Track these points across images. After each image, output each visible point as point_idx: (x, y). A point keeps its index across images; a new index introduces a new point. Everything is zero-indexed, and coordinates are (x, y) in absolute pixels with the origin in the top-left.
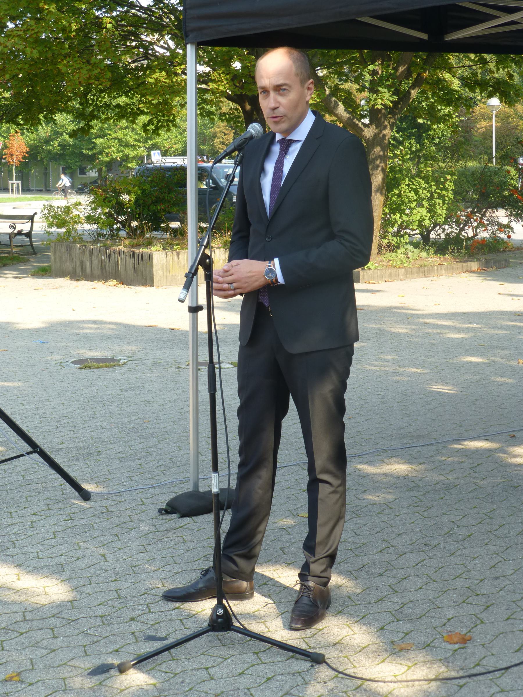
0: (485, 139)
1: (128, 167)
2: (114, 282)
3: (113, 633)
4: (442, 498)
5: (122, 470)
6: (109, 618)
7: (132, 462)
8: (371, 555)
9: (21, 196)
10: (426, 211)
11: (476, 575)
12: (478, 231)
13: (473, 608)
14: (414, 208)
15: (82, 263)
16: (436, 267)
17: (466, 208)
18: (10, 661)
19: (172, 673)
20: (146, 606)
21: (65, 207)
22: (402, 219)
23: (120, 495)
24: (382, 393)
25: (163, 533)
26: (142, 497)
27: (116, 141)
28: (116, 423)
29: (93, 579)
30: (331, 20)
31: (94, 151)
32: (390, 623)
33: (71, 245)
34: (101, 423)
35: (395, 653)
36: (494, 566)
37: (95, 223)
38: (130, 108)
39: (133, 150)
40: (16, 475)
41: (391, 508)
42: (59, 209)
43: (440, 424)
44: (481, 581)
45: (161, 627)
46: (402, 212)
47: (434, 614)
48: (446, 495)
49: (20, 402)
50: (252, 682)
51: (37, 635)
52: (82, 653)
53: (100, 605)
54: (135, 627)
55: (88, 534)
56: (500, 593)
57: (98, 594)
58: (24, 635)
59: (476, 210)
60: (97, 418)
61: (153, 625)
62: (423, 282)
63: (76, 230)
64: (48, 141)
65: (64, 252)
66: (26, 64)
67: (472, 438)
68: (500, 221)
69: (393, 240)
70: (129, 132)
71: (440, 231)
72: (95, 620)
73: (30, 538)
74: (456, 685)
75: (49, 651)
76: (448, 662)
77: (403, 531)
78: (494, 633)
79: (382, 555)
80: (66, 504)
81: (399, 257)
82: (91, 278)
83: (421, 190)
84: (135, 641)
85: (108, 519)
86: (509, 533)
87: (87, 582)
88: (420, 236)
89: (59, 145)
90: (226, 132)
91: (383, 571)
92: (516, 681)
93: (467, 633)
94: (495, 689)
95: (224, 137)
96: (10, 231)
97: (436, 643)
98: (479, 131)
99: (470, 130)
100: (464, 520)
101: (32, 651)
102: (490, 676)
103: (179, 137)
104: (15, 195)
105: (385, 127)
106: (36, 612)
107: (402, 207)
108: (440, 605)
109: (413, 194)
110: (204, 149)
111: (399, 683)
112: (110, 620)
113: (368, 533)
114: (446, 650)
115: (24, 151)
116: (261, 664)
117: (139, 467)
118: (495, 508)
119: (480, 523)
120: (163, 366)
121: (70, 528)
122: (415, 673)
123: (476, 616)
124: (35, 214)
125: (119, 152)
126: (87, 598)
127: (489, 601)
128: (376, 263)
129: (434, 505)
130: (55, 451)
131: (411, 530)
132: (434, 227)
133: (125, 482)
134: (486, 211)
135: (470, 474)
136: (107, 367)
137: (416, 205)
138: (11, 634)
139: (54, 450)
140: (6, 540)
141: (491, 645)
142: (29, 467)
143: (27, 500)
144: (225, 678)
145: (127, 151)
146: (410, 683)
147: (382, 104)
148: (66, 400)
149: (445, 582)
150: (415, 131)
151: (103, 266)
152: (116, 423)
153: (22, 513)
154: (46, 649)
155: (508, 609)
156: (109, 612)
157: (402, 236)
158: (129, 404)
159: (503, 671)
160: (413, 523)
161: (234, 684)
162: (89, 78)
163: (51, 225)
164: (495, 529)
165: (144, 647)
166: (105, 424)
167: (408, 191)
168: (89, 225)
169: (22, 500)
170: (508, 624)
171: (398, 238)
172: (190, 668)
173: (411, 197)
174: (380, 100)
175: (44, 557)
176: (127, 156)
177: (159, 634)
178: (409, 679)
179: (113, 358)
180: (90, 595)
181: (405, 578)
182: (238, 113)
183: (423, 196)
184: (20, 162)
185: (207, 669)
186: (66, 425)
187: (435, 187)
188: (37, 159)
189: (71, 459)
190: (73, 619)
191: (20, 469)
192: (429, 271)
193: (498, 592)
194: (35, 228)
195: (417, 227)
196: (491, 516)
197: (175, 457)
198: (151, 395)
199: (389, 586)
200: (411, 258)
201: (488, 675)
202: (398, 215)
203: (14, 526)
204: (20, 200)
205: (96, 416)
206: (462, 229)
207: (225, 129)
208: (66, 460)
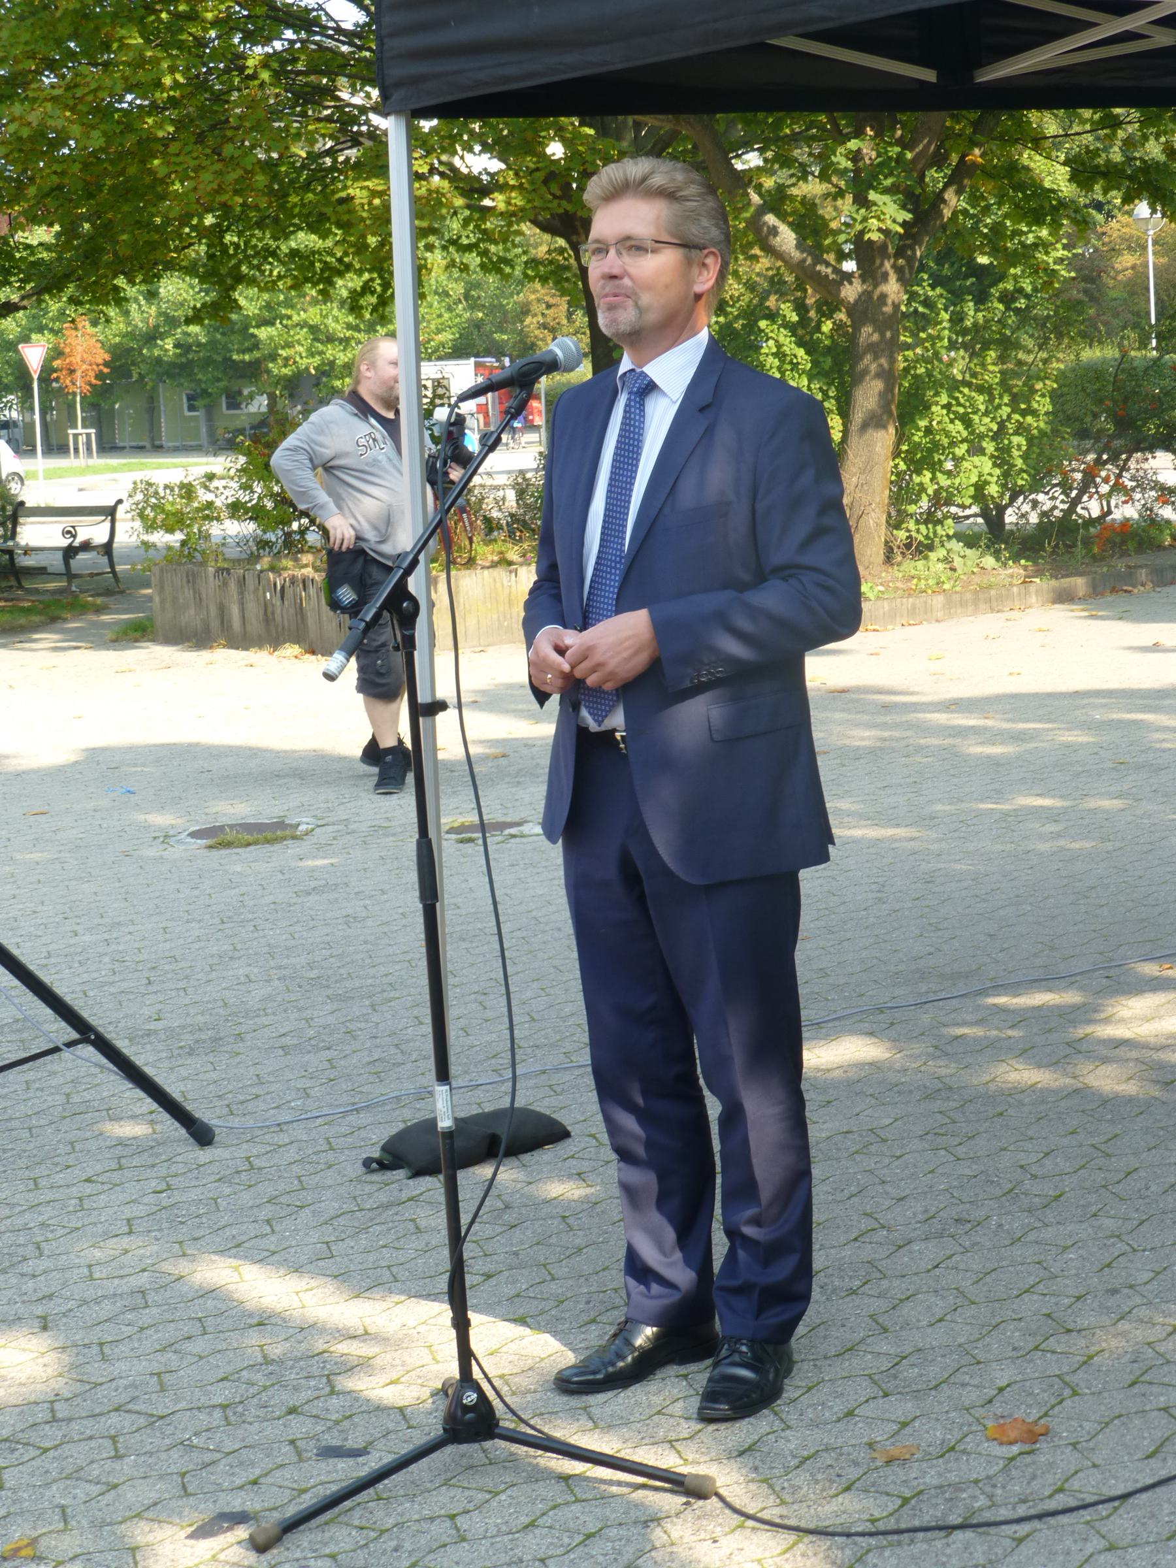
0: (1132, 294)
1: (332, 387)
2: (295, 649)
3: (249, 1441)
4: (1001, 1114)
5: (288, 1075)
6: (240, 1409)
7: (312, 1055)
8: (834, 1247)
9: (97, 461)
10: (990, 464)
11: (1066, 1286)
12: (1113, 503)
13: (1057, 1361)
14: (963, 458)
15: (222, 611)
16: (1015, 589)
17: (1086, 452)
18: (16, 1514)
19: (373, 1530)
20: (324, 1380)
21: (182, 486)
22: (938, 483)
23: (281, 1130)
24: (880, 879)
25: (371, 1214)
26: (329, 1135)
27: (305, 330)
28: (280, 967)
29: (210, 1322)
30: (697, 50)
31: (257, 354)
32: (867, 1401)
33: (196, 569)
34: (247, 970)
35: (877, 1468)
36: (1109, 1266)
37: (251, 519)
38: (320, 261)
39: (345, 350)
40: (52, 1094)
41: (884, 1141)
42: (168, 491)
43: (1005, 946)
44: (1078, 1298)
45: (355, 1425)
46: (935, 467)
47: (967, 1377)
48: (1010, 1106)
49: (68, 928)
50: (551, 1544)
51: (77, 1454)
52: (177, 1491)
53: (222, 1380)
54: (299, 1427)
55: (204, 1220)
56: (1120, 1325)
57: (219, 1356)
58: (51, 1454)
59: (1105, 457)
60: (239, 958)
61: (337, 1422)
62: (987, 623)
63: (207, 537)
64: (152, 337)
65: (182, 587)
66: (74, 161)
67: (1018, 984)
68: (1161, 478)
69: (918, 531)
70: (332, 309)
71: (1026, 508)
72: (210, 1414)
73: (74, 1234)
74: (1009, 1537)
75: (104, 1488)
76: (994, 1486)
77: (908, 1192)
78: (1102, 1416)
79: (859, 1247)
80: (158, 1155)
81: (932, 569)
82: (241, 641)
83: (976, 418)
84: (296, 1459)
85: (250, 1186)
86: (1147, 1189)
87: (196, 1329)
88: (980, 520)
89: (176, 346)
90: (552, 301)
91: (858, 1283)
92: (1144, 1524)
93: (1040, 1418)
94: (1096, 1543)
95: (546, 312)
96: (64, 542)
97: (969, 1444)
98: (1120, 277)
99: (1100, 277)
100: (1046, 1162)
101: (66, 1488)
102: (1086, 1515)
103: (446, 316)
104: (82, 461)
105: (885, 277)
106: (79, 1399)
107: (936, 457)
108: (981, 1357)
109: (959, 426)
110: (503, 340)
111: (880, 1537)
112: (242, 1415)
113: (830, 1198)
114: (990, 1459)
115: (100, 361)
116: (575, 1502)
117: (326, 1065)
118: (1118, 1132)
119: (1083, 1167)
120: (394, 835)
121: (165, 1208)
122: (918, 1512)
123: (1062, 1380)
124: (120, 502)
125: (312, 355)
126: (194, 1367)
127: (1093, 1344)
128: (881, 584)
129: (982, 1130)
130: (142, 1037)
131: (926, 1189)
132: (1013, 499)
133: (293, 1100)
134: (1128, 459)
135: (1066, 1056)
136: (268, 841)
137: (968, 451)
138: (22, 1451)
139: (140, 1033)
140: (22, 1240)
141: (1091, 1444)
142: (82, 1074)
143: (73, 1148)
144: (492, 1537)
145: (331, 352)
146: (906, 1535)
147: (880, 230)
148: (173, 920)
149: (997, 1305)
150: (973, 284)
151: (269, 614)
152: (280, 967)
153: (60, 1178)
154: (98, 1483)
155: (1135, 1361)
156: (242, 1396)
157: (940, 522)
158: (312, 923)
159: (1116, 1504)
160: (932, 1172)
161: (512, 1549)
162: (220, 190)
163: (150, 527)
164: (1116, 1179)
165: (315, 1473)
166: (256, 970)
167: (946, 419)
168: (236, 522)
169: (63, 1149)
170: (1134, 1396)
171: (930, 526)
172: (416, 1517)
173: (954, 434)
174: (874, 221)
175: (104, 1276)
176: (332, 363)
177: (350, 1442)
178: (903, 1526)
179: (283, 822)
180: (201, 1358)
181: (908, 1298)
182: (565, 259)
183: (982, 429)
184: (90, 384)
185: (452, 1517)
186: (169, 976)
187: (1008, 410)
188: (131, 376)
189: (176, 1052)
190: (161, 1414)
191: (62, 1080)
192: (1000, 598)
193: (1115, 1324)
194: (118, 538)
195: (970, 501)
196: (1108, 1151)
197: (408, 1041)
198: (362, 903)
199: (871, 1316)
200: (960, 571)
201: (1082, 1512)
202: (928, 475)
203: (41, 1209)
204: (96, 471)
205: (237, 954)
206: (1075, 502)
207: (547, 294)
208: (165, 1055)
